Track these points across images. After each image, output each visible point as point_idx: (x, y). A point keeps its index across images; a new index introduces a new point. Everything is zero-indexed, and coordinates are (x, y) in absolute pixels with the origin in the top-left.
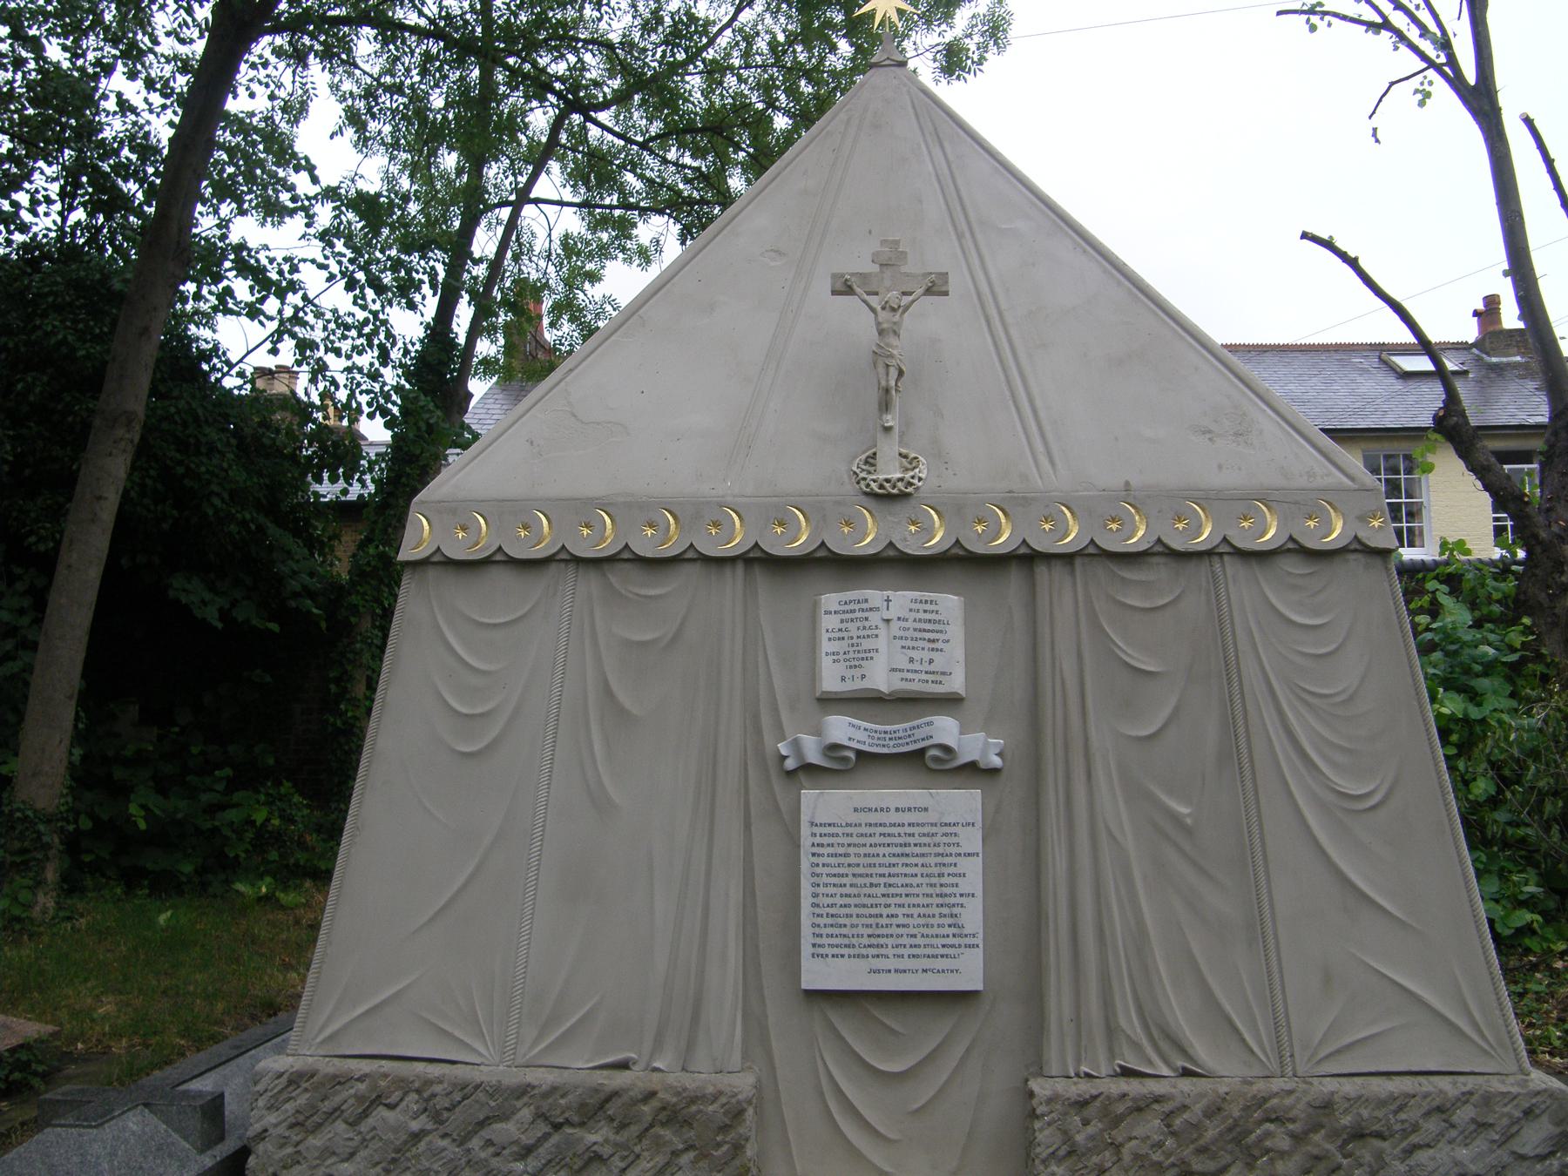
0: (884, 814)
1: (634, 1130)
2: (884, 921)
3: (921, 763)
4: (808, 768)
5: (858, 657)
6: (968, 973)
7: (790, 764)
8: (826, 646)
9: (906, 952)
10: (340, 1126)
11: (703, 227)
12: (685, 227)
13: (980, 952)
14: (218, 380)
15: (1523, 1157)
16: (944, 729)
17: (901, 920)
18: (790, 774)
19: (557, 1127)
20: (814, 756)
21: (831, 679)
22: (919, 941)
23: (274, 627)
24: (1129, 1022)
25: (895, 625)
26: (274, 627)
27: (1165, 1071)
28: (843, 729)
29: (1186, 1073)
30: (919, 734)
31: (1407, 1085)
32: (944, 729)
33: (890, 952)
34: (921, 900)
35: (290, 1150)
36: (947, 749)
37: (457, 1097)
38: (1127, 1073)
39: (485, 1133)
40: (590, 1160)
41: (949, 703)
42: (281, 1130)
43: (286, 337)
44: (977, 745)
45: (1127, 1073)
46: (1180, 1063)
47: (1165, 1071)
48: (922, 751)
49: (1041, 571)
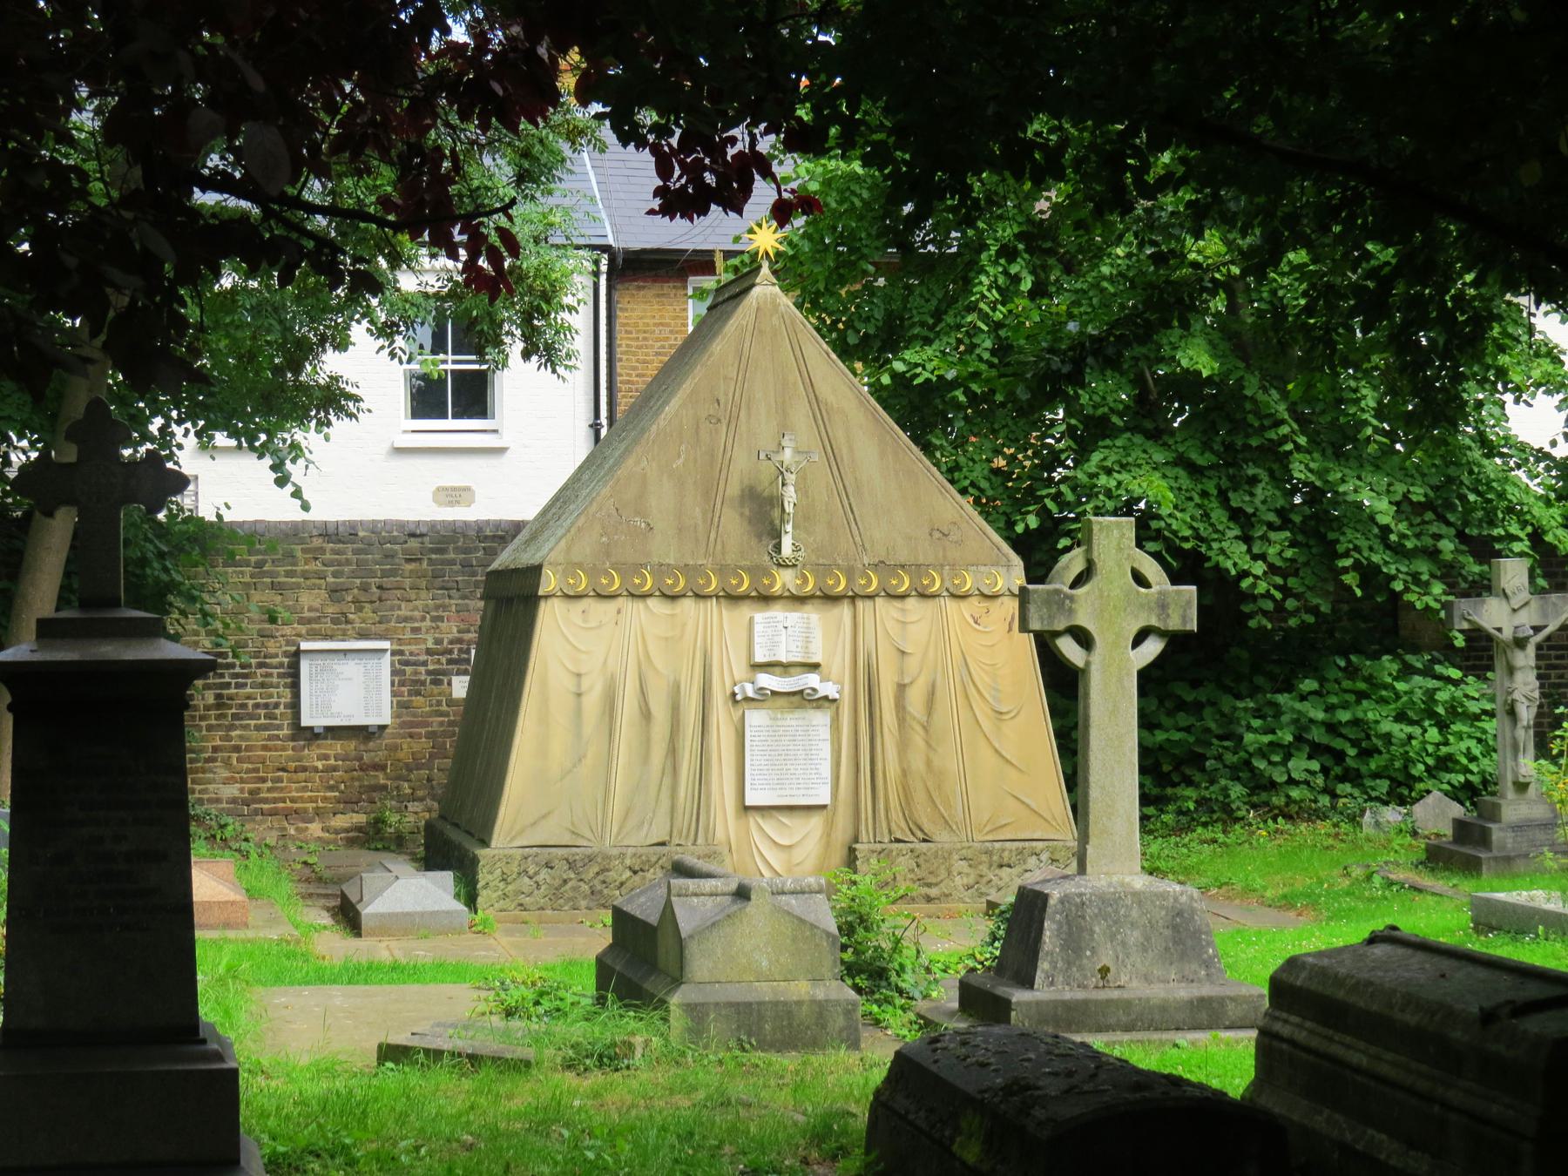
0: (585, 683)
3: (802, 699)
4: (747, 699)
5: (774, 645)
6: (824, 797)
10: (526, 880)
14: (368, 313)
19: (635, 872)
20: (750, 694)
21: (760, 657)
23: (1359, 593)
24: (896, 815)
26: (1359, 593)
27: (912, 838)
28: (767, 681)
29: (925, 841)
31: (1020, 844)
32: (812, 680)
36: (814, 690)
38: (898, 841)
39: (601, 877)
41: (815, 667)
43: (268, 460)
44: (829, 690)
45: (898, 841)
46: (921, 836)
48: (801, 692)
49: (860, 604)
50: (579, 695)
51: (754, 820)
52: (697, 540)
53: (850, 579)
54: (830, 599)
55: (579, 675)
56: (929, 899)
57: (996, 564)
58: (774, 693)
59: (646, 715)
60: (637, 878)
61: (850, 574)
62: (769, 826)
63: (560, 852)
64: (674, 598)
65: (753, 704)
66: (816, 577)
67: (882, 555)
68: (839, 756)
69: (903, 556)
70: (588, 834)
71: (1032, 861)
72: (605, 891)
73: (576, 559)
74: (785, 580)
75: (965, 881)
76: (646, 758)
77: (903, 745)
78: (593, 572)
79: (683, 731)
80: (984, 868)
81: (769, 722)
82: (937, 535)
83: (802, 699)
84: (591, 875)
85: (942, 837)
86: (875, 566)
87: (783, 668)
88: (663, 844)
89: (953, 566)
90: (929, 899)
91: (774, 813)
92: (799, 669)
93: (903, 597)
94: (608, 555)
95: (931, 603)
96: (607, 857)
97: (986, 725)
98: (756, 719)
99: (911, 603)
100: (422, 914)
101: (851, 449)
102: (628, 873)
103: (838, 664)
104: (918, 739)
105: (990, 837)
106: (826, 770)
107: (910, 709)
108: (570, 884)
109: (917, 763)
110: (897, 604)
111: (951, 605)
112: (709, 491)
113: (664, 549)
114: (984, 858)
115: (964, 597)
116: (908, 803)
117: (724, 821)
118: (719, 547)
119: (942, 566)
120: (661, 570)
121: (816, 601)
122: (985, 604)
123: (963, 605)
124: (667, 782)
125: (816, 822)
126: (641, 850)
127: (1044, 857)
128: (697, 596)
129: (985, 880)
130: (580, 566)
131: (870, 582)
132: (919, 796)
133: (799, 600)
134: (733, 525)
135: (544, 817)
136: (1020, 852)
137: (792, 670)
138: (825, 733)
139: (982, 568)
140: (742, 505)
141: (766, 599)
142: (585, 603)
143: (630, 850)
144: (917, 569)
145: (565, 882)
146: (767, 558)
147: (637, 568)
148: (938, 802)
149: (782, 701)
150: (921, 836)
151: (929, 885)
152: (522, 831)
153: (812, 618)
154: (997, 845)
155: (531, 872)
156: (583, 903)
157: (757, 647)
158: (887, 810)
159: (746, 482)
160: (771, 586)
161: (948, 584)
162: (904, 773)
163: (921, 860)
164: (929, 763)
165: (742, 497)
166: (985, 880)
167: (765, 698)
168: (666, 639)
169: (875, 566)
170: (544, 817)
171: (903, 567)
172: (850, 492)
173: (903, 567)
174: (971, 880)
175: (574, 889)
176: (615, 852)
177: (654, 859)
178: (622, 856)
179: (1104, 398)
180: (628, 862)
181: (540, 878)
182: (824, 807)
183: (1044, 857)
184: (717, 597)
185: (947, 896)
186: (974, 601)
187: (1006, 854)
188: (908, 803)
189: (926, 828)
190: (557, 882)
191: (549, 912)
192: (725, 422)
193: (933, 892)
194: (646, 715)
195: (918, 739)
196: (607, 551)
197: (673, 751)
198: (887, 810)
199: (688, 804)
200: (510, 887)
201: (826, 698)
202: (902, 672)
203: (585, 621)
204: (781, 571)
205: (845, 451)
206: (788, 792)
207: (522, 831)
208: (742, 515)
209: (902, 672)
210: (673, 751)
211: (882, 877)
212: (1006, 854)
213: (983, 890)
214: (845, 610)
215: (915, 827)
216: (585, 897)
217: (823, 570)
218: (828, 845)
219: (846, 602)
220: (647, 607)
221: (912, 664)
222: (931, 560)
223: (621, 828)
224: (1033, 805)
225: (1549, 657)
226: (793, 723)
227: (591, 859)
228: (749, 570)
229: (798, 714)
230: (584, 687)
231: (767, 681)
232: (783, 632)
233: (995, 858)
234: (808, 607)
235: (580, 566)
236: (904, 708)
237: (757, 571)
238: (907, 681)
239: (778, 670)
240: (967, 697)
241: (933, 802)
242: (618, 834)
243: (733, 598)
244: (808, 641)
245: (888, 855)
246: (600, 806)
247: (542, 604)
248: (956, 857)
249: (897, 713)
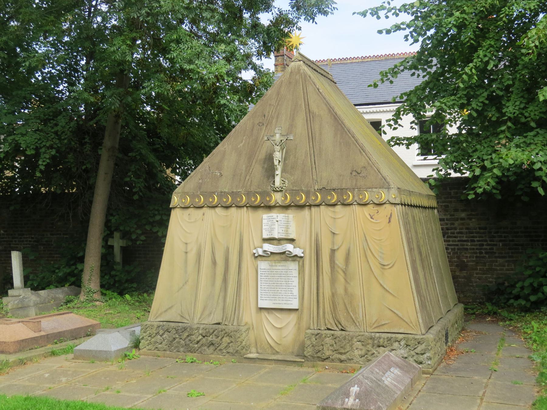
1: (220, 338)
2: (276, 292)
3: (285, 256)
5: (271, 230)
6: (295, 304)
7: (256, 255)
8: (264, 227)
9: (281, 299)
10: (159, 336)
11: (245, 115)
12: (320, 12)
13: (297, 300)
15: (417, 354)
16: (289, 247)
17: (280, 292)
18: (257, 257)
19: (204, 337)
21: (265, 236)
22: (284, 297)
24: (329, 317)
25: (279, 222)
27: (336, 328)
28: (269, 247)
29: (342, 330)
30: (284, 248)
31: (389, 335)
32: (289, 247)
33: (277, 299)
34: (284, 287)
35: (149, 342)
36: (290, 252)
37: (183, 330)
38: (329, 329)
39: (189, 338)
40: (211, 345)
41: (292, 241)
42: (147, 337)
44: (298, 252)
45: (329, 329)
46: (340, 327)
47: (336, 328)
48: (285, 252)
49: (313, 209)
50: (186, 253)
51: (264, 314)
52: (240, 180)
53: (307, 197)
54: (301, 207)
55: (186, 244)
56: (341, 361)
57: (382, 187)
58: (272, 253)
59: (214, 263)
60: (204, 339)
61: (308, 194)
62: (271, 317)
63: (172, 325)
64: (227, 207)
65: (264, 258)
66: (291, 196)
67: (324, 183)
68: (304, 285)
69: (335, 185)
70: (187, 317)
71: (396, 345)
72: (191, 345)
73: (186, 190)
74: (277, 198)
75: (360, 352)
76: (213, 284)
77: (333, 281)
78: (193, 196)
79: (228, 271)
80: (369, 347)
81: (269, 267)
82: (354, 173)
83: (285, 256)
84: (185, 336)
85: (351, 328)
86: (320, 190)
87: (279, 241)
88: (219, 324)
89: (359, 189)
90: (341, 361)
91: (274, 312)
92: (285, 241)
93: (334, 205)
94: (200, 188)
95: (348, 209)
96: (191, 329)
97: (377, 271)
98: (263, 265)
99: (339, 208)
100: (96, 351)
101: (321, 134)
102: (201, 337)
103: (304, 239)
104: (341, 277)
105: (376, 330)
106: (296, 291)
107: (337, 262)
108: (177, 340)
109: (340, 290)
110: (331, 209)
111: (356, 208)
112: (251, 157)
113: (225, 185)
114: (370, 341)
115: (365, 205)
116: (334, 310)
117: (248, 316)
118: (249, 183)
119: (354, 189)
120: (222, 195)
121: (293, 208)
122: (377, 208)
123: (365, 209)
124: (222, 294)
125: (293, 317)
126: (207, 326)
127: (403, 343)
128: (237, 206)
129: (370, 353)
130: (187, 194)
131: (317, 197)
132: (340, 307)
133: (286, 207)
134: (258, 170)
135: (170, 308)
136: (389, 339)
137: (282, 242)
138: (295, 273)
139: (374, 190)
140: (264, 163)
141: (270, 208)
142: (190, 210)
143: (202, 326)
144: (341, 191)
145: (174, 339)
146: (269, 187)
147: (212, 194)
148: (350, 310)
149: (277, 257)
150: (340, 327)
151: (341, 354)
152: (161, 314)
153: (291, 215)
154: (378, 335)
155: (161, 334)
156: (182, 349)
157: (264, 231)
158: (324, 313)
159: (269, 152)
160: (270, 201)
161: (356, 198)
162: (333, 295)
163: (337, 341)
164: (346, 290)
165: (265, 159)
166: (370, 353)
167: (267, 256)
168: (224, 227)
169: (320, 190)
170: (170, 308)
171: (334, 190)
172: (316, 154)
173: (334, 190)
174: (363, 352)
175: (179, 342)
176: (195, 327)
177: (211, 331)
178: (198, 329)
179: (530, 114)
180: (201, 332)
181: (164, 336)
182: (297, 310)
183: (403, 343)
184: (247, 207)
185: (350, 360)
186: (370, 207)
187: (381, 340)
188: (334, 310)
189: (343, 323)
190: (171, 339)
191: (168, 352)
192: (265, 125)
193: (343, 357)
194: (214, 263)
195: (341, 277)
196: (200, 187)
197: (225, 280)
198: (324, 313)
199: (231, 306)
200: (153, 340)
201: (296, 256)
202: (333, 243)
203: (189, 219)
204: (276, 194)
205: (317, 135)
206: (278, 302)
207: (161, 314)
208: (263, 167)
209: (333, 243)
210: (225, 280)
211: (317, 348)
212: (381, 340)
213: (369, 358)
214: (306, 211)
215: (338, 322)
216: (183, 347)
217: (295, 193)
218: (299, 329)
219: (307, 208)
220: (216, 212)
221: (339, 239)
222: (349, 186)
223: (202, 314)
224: (400, 315)
225: (449, 241)
226: (280, 268)
227: (185, 329)
228: (260, 194)
229: (283, 263)
230: (188, 250)
231: (269, 247)
232: (275, 223)
233: (376, 342)
234: (289, 211)
235: (187, 194)
236: (334, 262)
237: (265, 194)
238: (336, 248)
239: (275, 242)
240: (366, 257)
241: (347, 310)
242: (200, 318)
243: (256, 207)
244: (287, 227)
245: (320, 337)
246: (193, 305)
247: (172, 211)
248: (355, 340)
249: (331, 263)
